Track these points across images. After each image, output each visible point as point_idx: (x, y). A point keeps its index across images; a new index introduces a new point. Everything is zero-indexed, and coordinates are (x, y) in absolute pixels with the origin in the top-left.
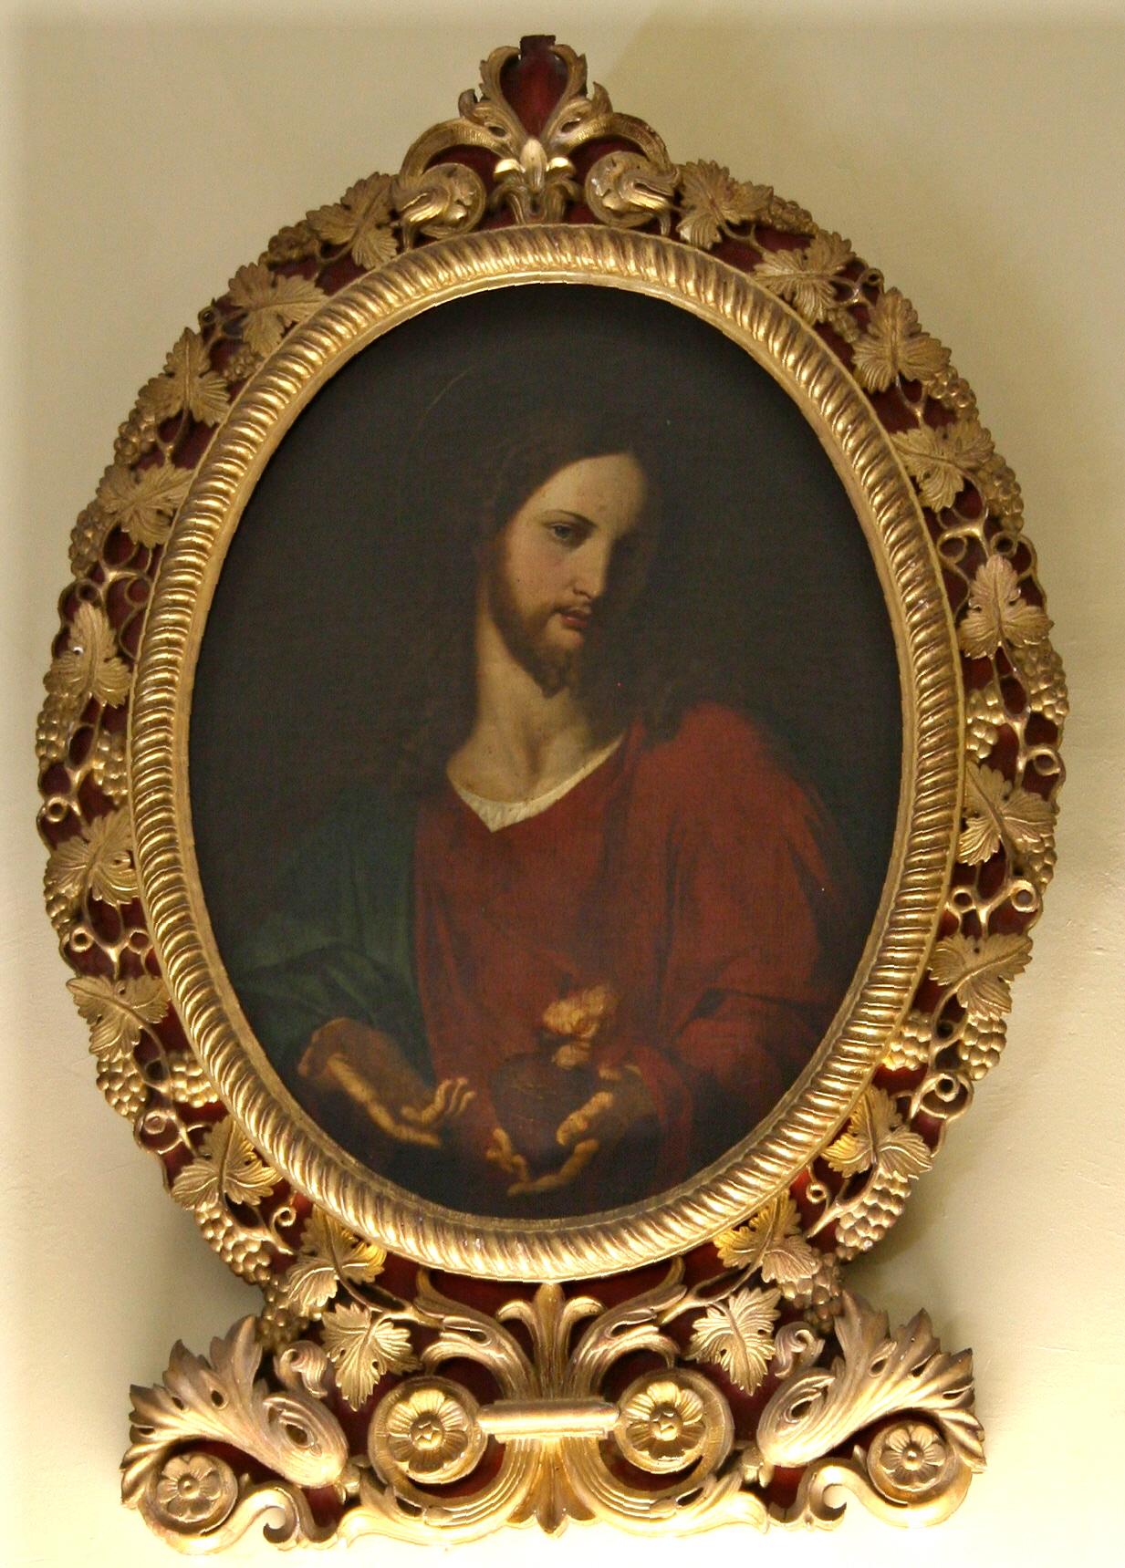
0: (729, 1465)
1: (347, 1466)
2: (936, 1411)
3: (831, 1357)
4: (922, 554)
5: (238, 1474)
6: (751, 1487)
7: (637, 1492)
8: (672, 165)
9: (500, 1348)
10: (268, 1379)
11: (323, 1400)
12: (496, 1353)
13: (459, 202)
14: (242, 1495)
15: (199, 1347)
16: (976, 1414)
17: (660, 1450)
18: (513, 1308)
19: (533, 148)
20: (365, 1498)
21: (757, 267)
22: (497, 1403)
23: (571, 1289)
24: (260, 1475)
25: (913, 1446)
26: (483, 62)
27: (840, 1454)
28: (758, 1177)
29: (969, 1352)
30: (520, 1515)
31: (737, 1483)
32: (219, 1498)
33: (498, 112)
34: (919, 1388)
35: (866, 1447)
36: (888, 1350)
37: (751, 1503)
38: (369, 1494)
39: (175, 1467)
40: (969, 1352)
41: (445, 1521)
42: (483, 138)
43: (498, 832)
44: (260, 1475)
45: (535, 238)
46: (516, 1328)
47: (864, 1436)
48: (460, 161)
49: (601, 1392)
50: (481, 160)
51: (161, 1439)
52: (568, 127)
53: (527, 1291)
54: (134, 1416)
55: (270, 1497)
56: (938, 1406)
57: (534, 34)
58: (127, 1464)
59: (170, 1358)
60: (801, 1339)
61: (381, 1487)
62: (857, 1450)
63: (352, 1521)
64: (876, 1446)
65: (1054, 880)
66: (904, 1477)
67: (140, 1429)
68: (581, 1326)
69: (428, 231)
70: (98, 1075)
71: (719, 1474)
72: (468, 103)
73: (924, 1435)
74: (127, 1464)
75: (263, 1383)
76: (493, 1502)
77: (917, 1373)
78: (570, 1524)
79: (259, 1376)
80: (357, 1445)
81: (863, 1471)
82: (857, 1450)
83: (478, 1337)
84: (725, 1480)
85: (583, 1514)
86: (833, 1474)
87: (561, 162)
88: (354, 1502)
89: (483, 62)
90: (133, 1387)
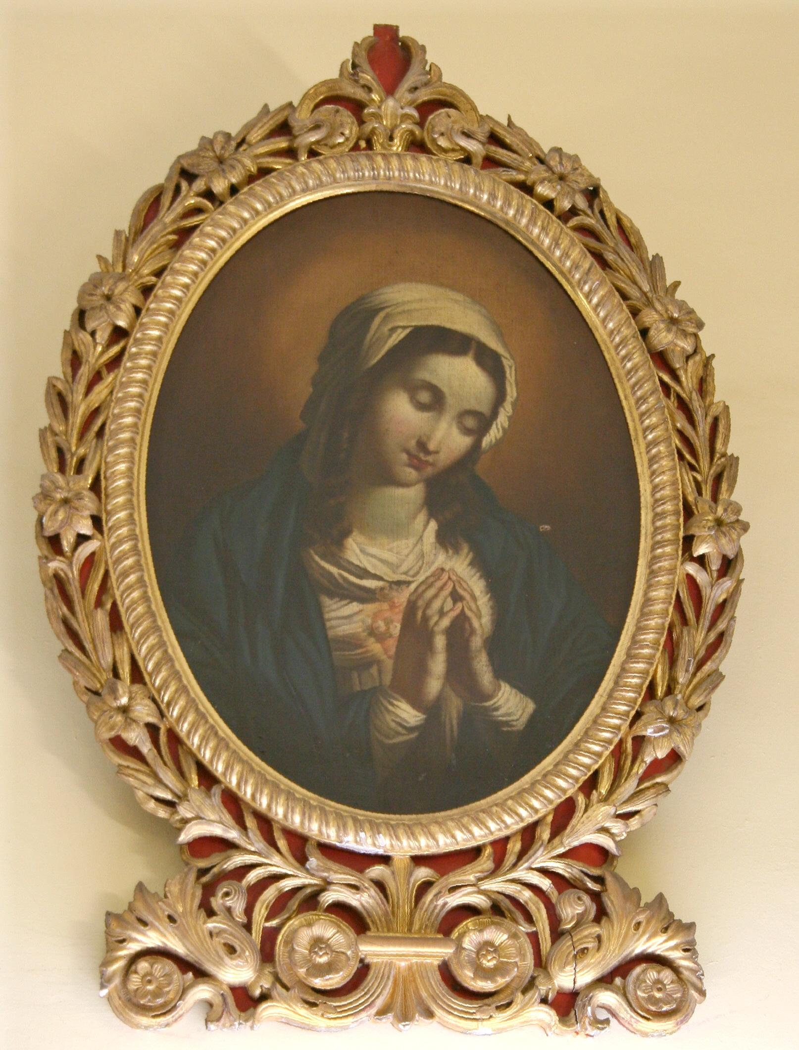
0: (531, 985)
1: (260, 972)
3: (602, 914)
6: (544, 1001)
7: (459, 998)
8: (481, 116)
15: (153, 887)
17: (482, 972)
18: (377, 871)
20: (274, 993)
23: (418, 860)
24: (201, 974)
25: (658, 981)
26: (356, 43)
27: (605, 981)
30: (382, 1013)
32: (172, 990)
33: (368, 77)
34: (666, 941)
35: (624, 976)
37: (548, 1015)
39: (143, 965)
40: (691, 927)
42: (359, 94)
44: (201, 974)
47: (623, 969)
48: (342, 106)
49: (439, 931)
51: (133, 948)
53: (385, 860)
54: (108, 933)
55: (203, 992)
56: (676, 955)
57: (387, 23)
63: (266, 1010)
65: (37, 580)
66: (652, 1000)
68: (426, 886)
70: (85, 705)
71: (525, 991)
73: (667, 975)
74: (106, 963)
75: (203, 914)
76: (362, 1000)
79: (200, 906)
80: (267, 954)
84: (529, 995)
85: (430, 1014)
86: (606, 997)
88: (265, 997)
89: (356, 43)
90: (108, 914)
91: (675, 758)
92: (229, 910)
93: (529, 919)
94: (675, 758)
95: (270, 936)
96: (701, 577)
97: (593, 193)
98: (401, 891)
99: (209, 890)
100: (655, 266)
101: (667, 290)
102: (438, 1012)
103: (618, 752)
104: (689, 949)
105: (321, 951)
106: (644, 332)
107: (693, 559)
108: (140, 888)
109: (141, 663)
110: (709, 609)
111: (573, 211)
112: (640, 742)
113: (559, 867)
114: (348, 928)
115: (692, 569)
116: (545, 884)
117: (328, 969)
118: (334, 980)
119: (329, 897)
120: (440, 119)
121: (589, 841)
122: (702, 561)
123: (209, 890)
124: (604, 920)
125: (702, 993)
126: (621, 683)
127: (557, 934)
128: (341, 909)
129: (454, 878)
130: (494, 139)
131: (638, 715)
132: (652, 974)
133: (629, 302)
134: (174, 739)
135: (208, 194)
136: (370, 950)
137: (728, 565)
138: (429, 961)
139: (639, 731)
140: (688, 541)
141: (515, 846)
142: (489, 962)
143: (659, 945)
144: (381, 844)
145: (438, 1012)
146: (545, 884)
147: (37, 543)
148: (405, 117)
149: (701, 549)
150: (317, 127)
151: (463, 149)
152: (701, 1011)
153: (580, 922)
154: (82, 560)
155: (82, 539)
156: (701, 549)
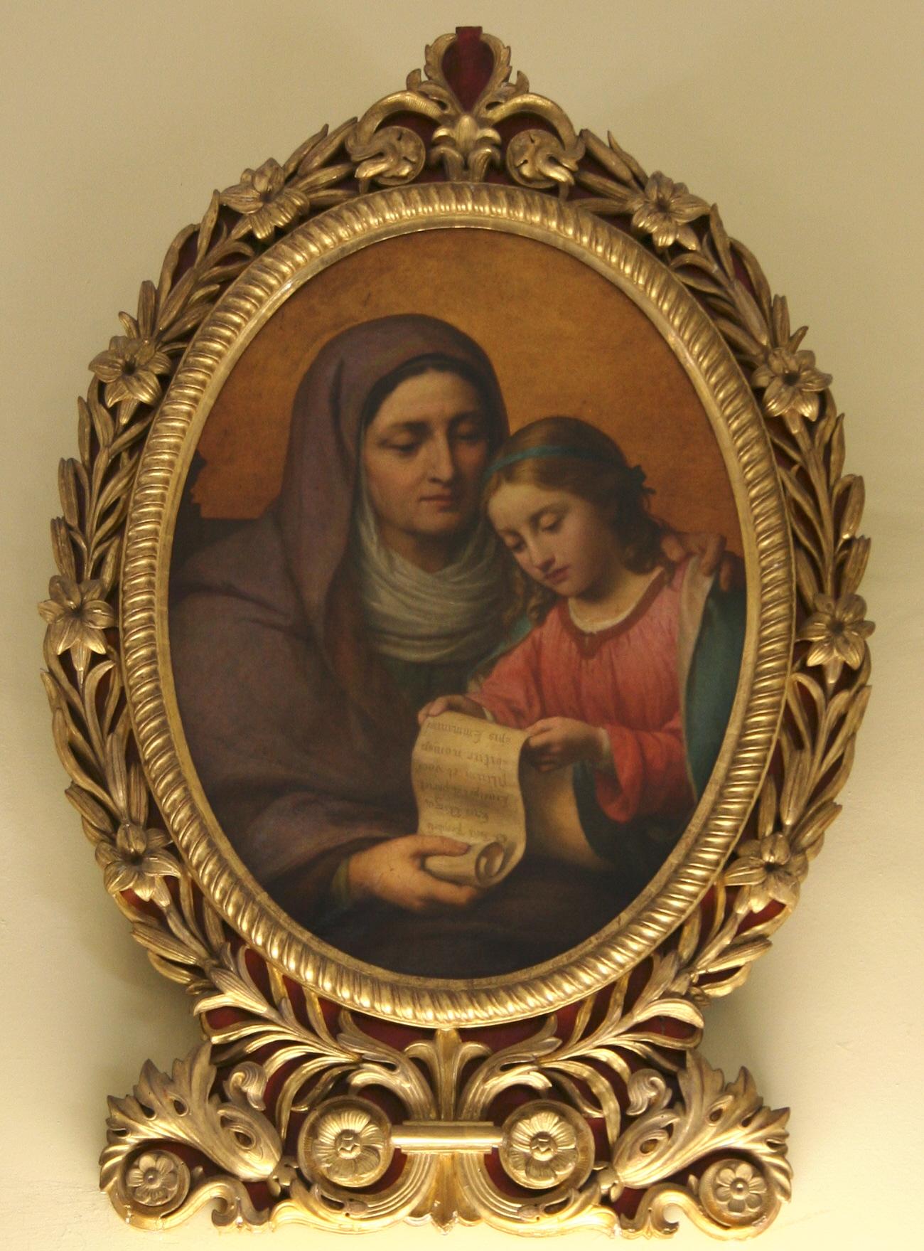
2: (760, 1156)
3: (678, 1102)
4: (770, 473)
5: (191, 1167)
6: (605, 1201)
9: (408, 1079)
10: (218, 1092)
11: (263, 1112)
12: (406, 1084)
13: (405, 159)
14: (195, 1185)
15: (163, 1067)
16: (791, 1181)
18: (420, 1048)
19: (466, 121)
20: (293, 1193)
21: (647, 484)
22: (407, 1123)
23: (466, 1034)
24: (215, 1171)
27: (677, 1180)
28: (624, 1149)
29: (785, 1111)
30: (416, 1213)
31: (596, 1200)
35: (699, 1176)
36: (725, 1103)
37: (603, 1216)
38: (299, 1188)
39: (146, 1161)
40: (785, 1111)
41: (363, 1215)
43: (415, 718)
44: (215, 1171)
45: (457, 999)
46: (424, 1067)
47: (699, 1166)
50: (424, 124)
51: (132, 1140)
52: (491, 106)
54: (110, 1121)
55: (213, 1190)
56: (762, 1150)
58: (104, 1158)
59: (180, 233)
60: (653, 1084)
61: (308, 1185)
62: (692, 1179)
63: (286, 1212)
64: (710, 1173)
67: (116, 1133)
69: (381, 181)
72: (412, 83)
73: (744, 1170)
74: (104, 1158)
75: (216, 1098)
77: (746, 1123)
78: (458, 1227)
80: (288, 1150)
81: (695, 1196)
82: (692, 1179)
83: (391, 1067)
85: (471, 1216)
86: (672, 1199)
87: (491, 133)
88: (285, 1195)
91: (774, 909)
92: (244, 1095)
93: (596, 1103)
94: (774, 909)
95: (296, 1121)
96: (816, 691)
97: (703, 225)
98: (448, 1074)
99: (223, 1071)
100: (773, 311)
101: (791, 339)
102: (484, 1213)
103: (707, 906)
104: (779, 1147)
105: (348, 1146)
106: (759, 393)
107: (805, 669)
108: (149, 1069)
109: (157, 800)
110: (826, 725)
111: (678, 248)
112: (734, 893)
113: (626, 1042)
114: (664, 1044)
115: (804, 679)
116: (619, 1064)
117: (354, 1166)
118: (368, 1178)
119: (359, 1079)
120: (525, 140)
121: (666, 1014)
122: (818, 673)
123: (223, 1071)
124: (678, 1106)
125: (786, 1193)
126: (711, 827)
127: (627, 1122)
128: (378, 1093)
129: (506, 1056)
130: (590, 162)
131: (734, 857)
132: (728, 1174)
133: (742, 357)
134: (198, 894)
135: (250, 238)
136: (401, 1141)
137: (850, 677)
138: (470, 1152)
139: (733, 878)
140: (804, 647)
141: (582, 1020)
142: (543, 1156)
143: (738, 1138)
144: (426, 1017)
145: (484, 1213)
146: (619, 1064)
147: (178, 236)
148: (485, 141)
149: (815, 659)
150: (380, 155)
151: (550, 179)
152: (786, 1210)
153: (652, 1107)
154: (95, 684)
155: (95, 659)
156: (815, 659)
